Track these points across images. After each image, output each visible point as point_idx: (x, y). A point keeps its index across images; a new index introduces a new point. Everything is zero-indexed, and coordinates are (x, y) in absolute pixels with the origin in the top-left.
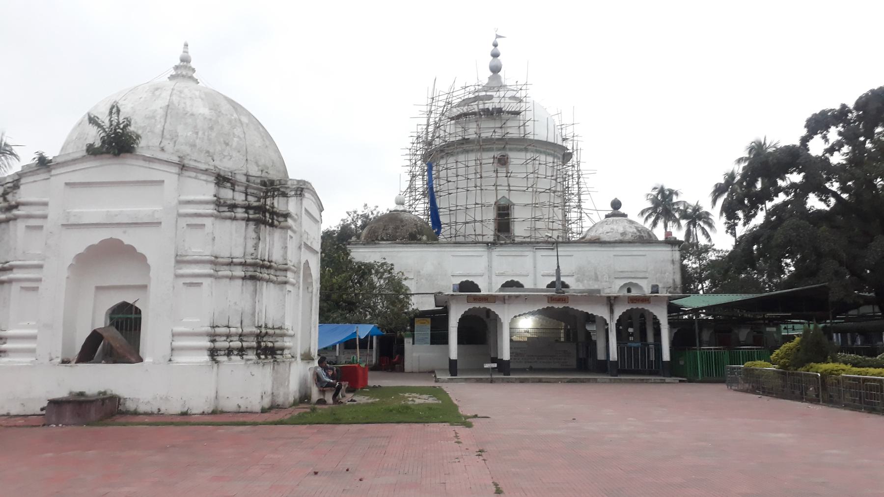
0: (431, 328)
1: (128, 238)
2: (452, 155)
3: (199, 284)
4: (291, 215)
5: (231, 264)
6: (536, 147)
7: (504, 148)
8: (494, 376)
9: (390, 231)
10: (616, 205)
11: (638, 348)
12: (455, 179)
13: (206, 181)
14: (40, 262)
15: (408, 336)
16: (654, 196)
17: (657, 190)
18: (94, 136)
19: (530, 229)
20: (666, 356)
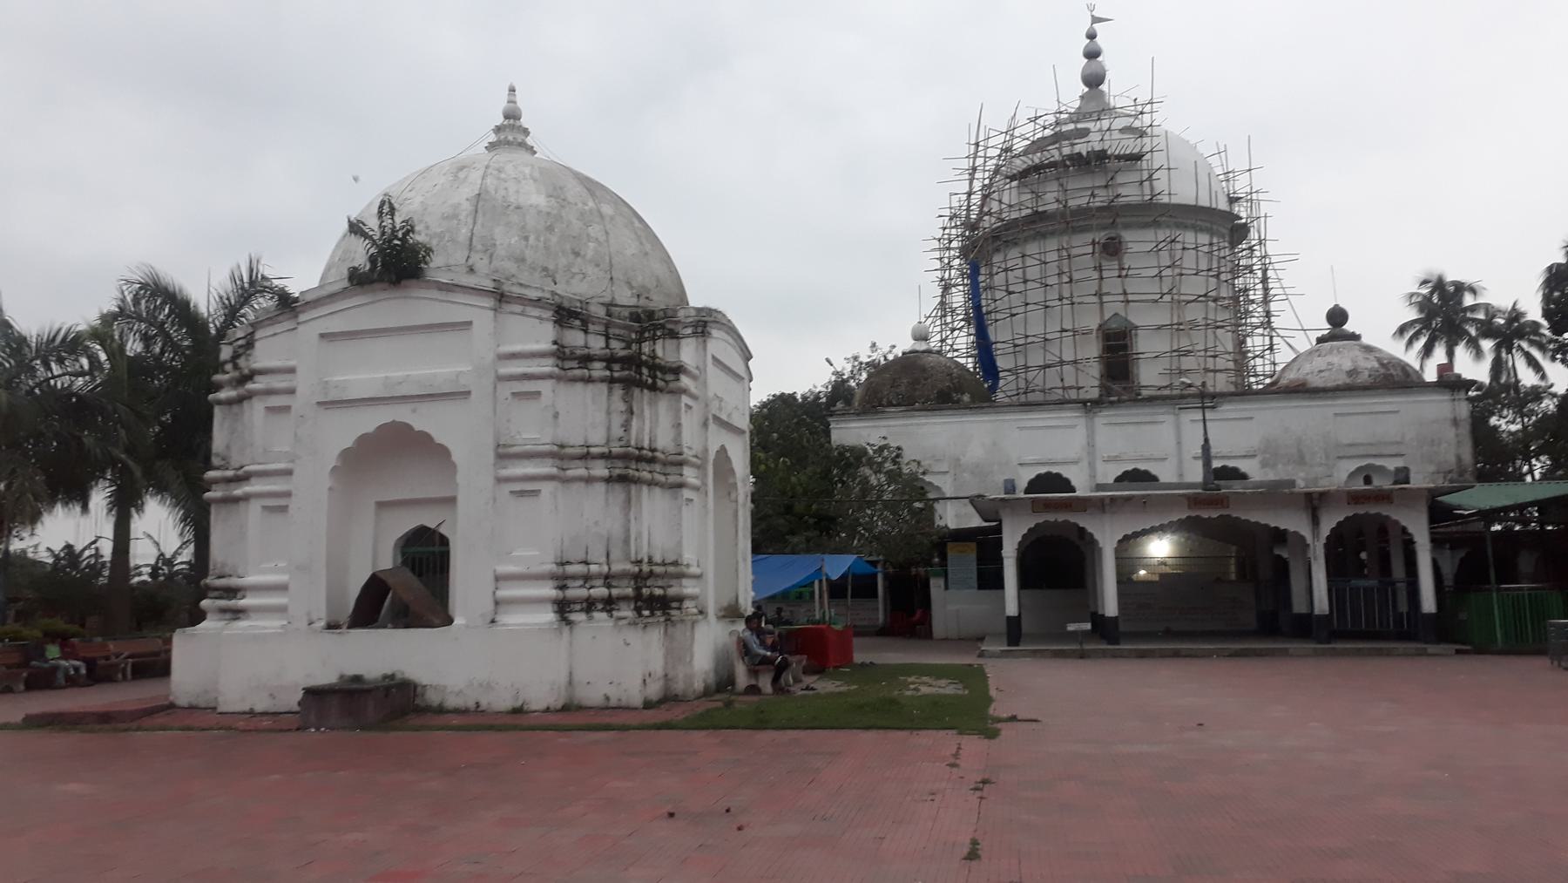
0: (977, 557)
1: (421, 419)
2: (1016, 244)
3: (535, 493)
4: (685, 369)
5: (586, 457)
6: (1175, 217)
7: (1113, 223)
8: (1087, 647)
9: (903, 388)
10: (1337, 317)
11: (1372, 589)
12: (1020, 288)
13: (539, 318)
14: (290, 466)
15: (937, 575)
16: (1424, 296)
17: (1430, 285)
18: (360, 253)
19: (1168, 372)
20: (1428, 603)
